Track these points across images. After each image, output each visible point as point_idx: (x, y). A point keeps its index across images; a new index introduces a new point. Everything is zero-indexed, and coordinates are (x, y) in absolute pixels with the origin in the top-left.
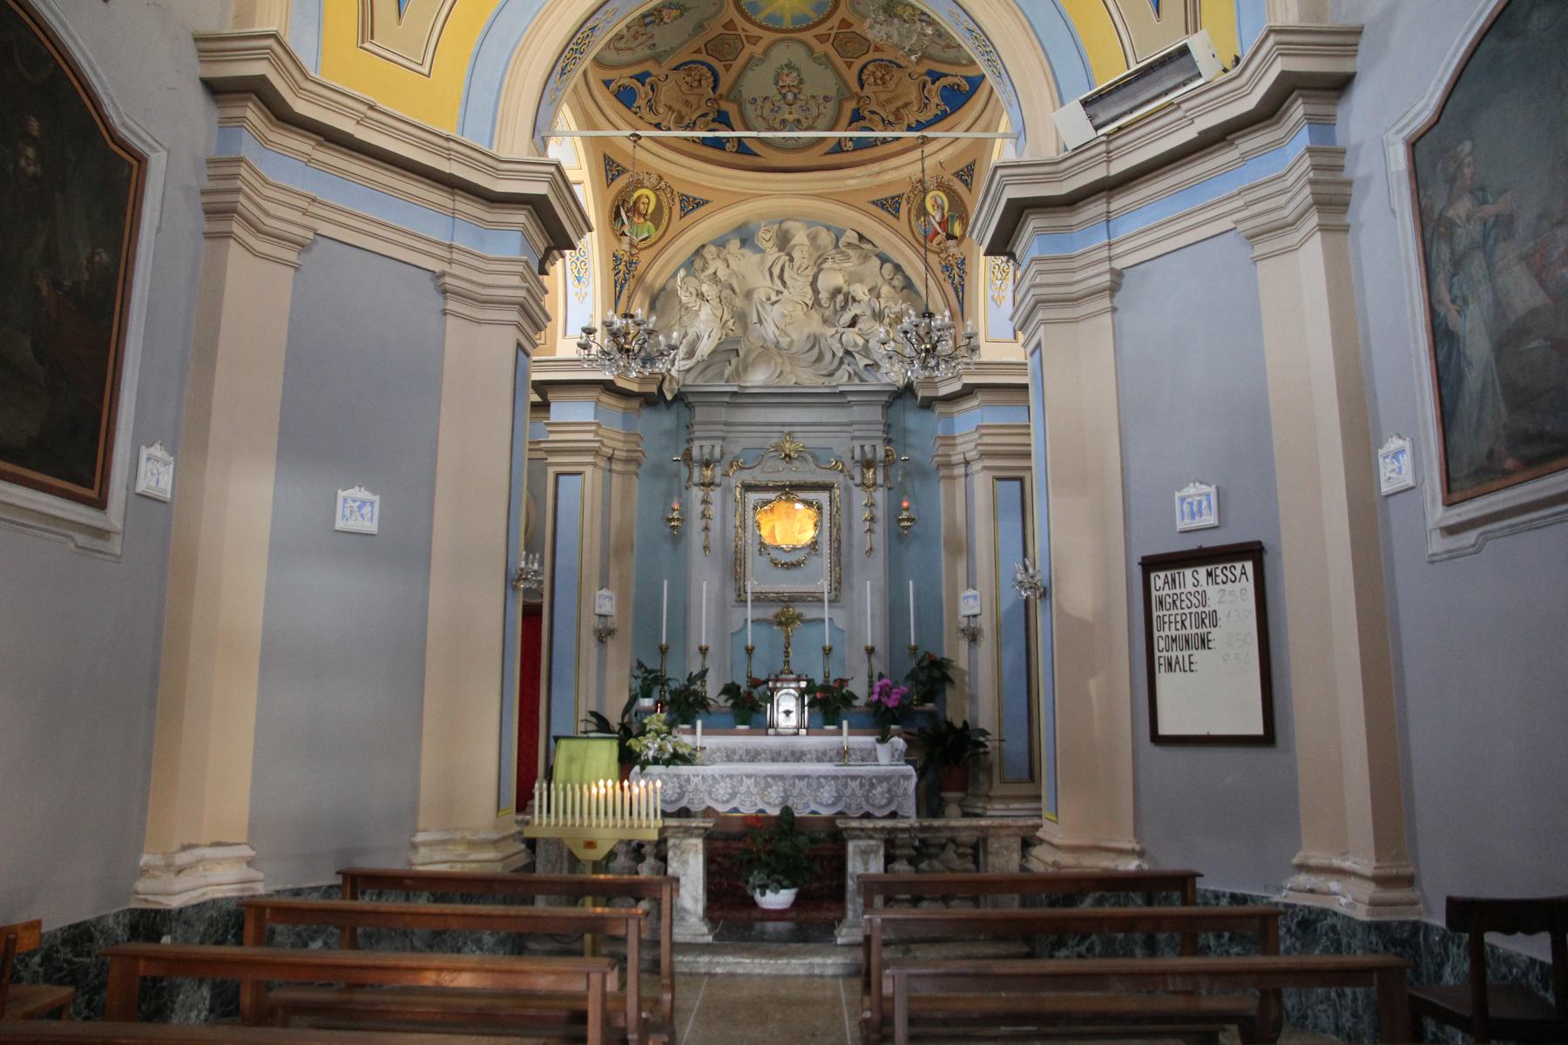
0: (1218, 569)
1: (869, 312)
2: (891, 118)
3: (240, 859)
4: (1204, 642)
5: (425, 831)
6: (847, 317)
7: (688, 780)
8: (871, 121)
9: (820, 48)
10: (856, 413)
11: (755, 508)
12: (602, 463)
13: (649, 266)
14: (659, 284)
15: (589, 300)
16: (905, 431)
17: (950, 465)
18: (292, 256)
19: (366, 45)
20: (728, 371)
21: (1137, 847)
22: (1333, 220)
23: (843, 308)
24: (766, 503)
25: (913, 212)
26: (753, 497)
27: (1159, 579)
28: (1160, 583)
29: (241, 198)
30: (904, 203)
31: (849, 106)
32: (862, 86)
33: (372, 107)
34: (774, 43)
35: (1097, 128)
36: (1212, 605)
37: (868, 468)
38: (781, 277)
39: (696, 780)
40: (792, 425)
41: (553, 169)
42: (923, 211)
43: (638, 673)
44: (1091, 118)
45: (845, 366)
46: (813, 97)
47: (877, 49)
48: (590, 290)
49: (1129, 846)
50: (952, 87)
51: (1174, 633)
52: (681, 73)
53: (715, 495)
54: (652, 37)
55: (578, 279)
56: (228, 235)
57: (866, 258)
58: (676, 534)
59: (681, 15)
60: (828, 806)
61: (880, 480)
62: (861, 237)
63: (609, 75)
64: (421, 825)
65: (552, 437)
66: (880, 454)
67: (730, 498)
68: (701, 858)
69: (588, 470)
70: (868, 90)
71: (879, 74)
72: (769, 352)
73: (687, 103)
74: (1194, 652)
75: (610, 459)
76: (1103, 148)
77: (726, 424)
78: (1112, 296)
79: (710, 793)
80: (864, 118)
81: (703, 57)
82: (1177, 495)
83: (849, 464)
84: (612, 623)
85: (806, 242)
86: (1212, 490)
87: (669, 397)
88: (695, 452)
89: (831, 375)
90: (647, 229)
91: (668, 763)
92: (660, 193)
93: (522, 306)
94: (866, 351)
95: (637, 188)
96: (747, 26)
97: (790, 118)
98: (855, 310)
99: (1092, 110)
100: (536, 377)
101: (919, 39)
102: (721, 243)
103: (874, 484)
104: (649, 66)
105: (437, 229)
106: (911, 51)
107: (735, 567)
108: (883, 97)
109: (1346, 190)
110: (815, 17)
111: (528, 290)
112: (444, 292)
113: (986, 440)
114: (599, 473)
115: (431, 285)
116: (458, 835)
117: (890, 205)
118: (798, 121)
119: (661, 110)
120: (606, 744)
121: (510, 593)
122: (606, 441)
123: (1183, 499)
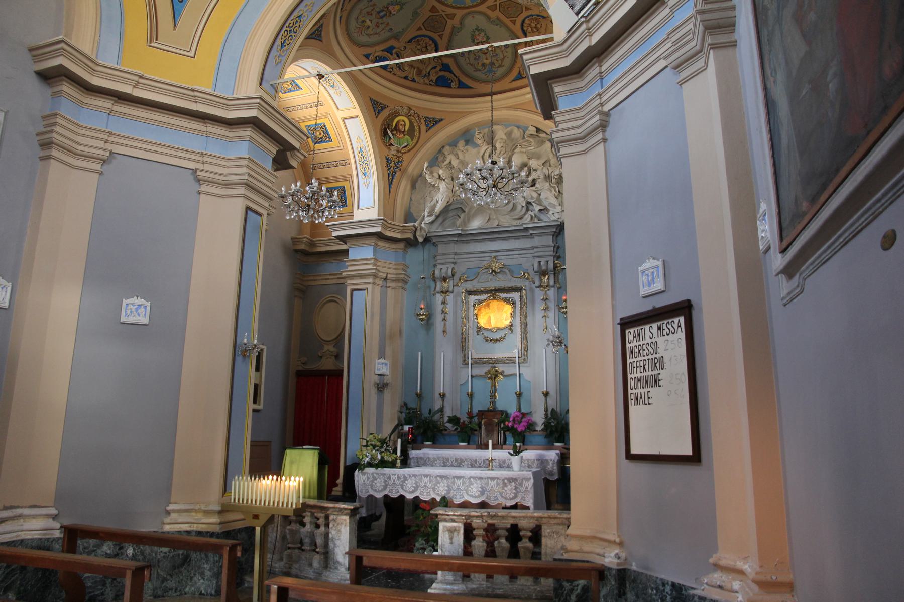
0: (664, 323)
1: (542, 177)
3: (48, 516)
4: (656, 381)
5: (175, 503)
7: (389, 478)
9: (493, 15)
10: (537, 241)
11: (474, 305)
13: (408, 165)
14: (416, 173)
15: (371, 187)
18: (98, 167)
19: (153, 44)
20: (458, 222)
21: (618, 540)
22: (722, 38)
24: (480, 302)
26: (473, 299)
27: (630, 333)
28: (631, 337)
29: (55, 135)
33: (141, 77)
34: (463, 18)
35: (577, 14)
36: (661, 352)
39: (394, 477)
43: (404, 410)
47: (527, 9)
48: (371, 180)
49: (611, 537)
51: (639, 375)
53: (450, 298)
54: (388, 24)
55: (364, 174)
56: (49, 157)
57: (543, 142)
58: (428, 321)
59: (401, 8)
60: (475, 497)
61: (552, 283)
62: (538, 130)
64: (172, 500)
65: (350, 268)
66: (551, 266)
67: (459, 300)
68: (348, 528)
69: (370, 287)
71: (533, 25)
74: (650, 389)
75: (386, 279)
76: (584, 26)
77: (456, 254)
79: (402, 486)
81: (424, 32)
82: (640, 269)
84: (387, 379)
85: (505, 137)
86: (659, 263)
87: (421, 240)
88: (437, 273)
89: (521, 218)
91: (377, 466)
93: (246, 184)
95: (396, 117)
96: (444, 8)
97: (487, 62)
98: (534, 175)
100: (334, 234)
102: (454, 144)
103: (548, 286)
104: (392, 42)
105: (196, 144)
107: (463, 343)
109: (731, 13)
112: (199, 180)
114: (378, 289)
115: (192, 177)
116: (197, 507)
119: (407, 68)
120: (311, 452)
121: (239, 359)
123: (643, 272)
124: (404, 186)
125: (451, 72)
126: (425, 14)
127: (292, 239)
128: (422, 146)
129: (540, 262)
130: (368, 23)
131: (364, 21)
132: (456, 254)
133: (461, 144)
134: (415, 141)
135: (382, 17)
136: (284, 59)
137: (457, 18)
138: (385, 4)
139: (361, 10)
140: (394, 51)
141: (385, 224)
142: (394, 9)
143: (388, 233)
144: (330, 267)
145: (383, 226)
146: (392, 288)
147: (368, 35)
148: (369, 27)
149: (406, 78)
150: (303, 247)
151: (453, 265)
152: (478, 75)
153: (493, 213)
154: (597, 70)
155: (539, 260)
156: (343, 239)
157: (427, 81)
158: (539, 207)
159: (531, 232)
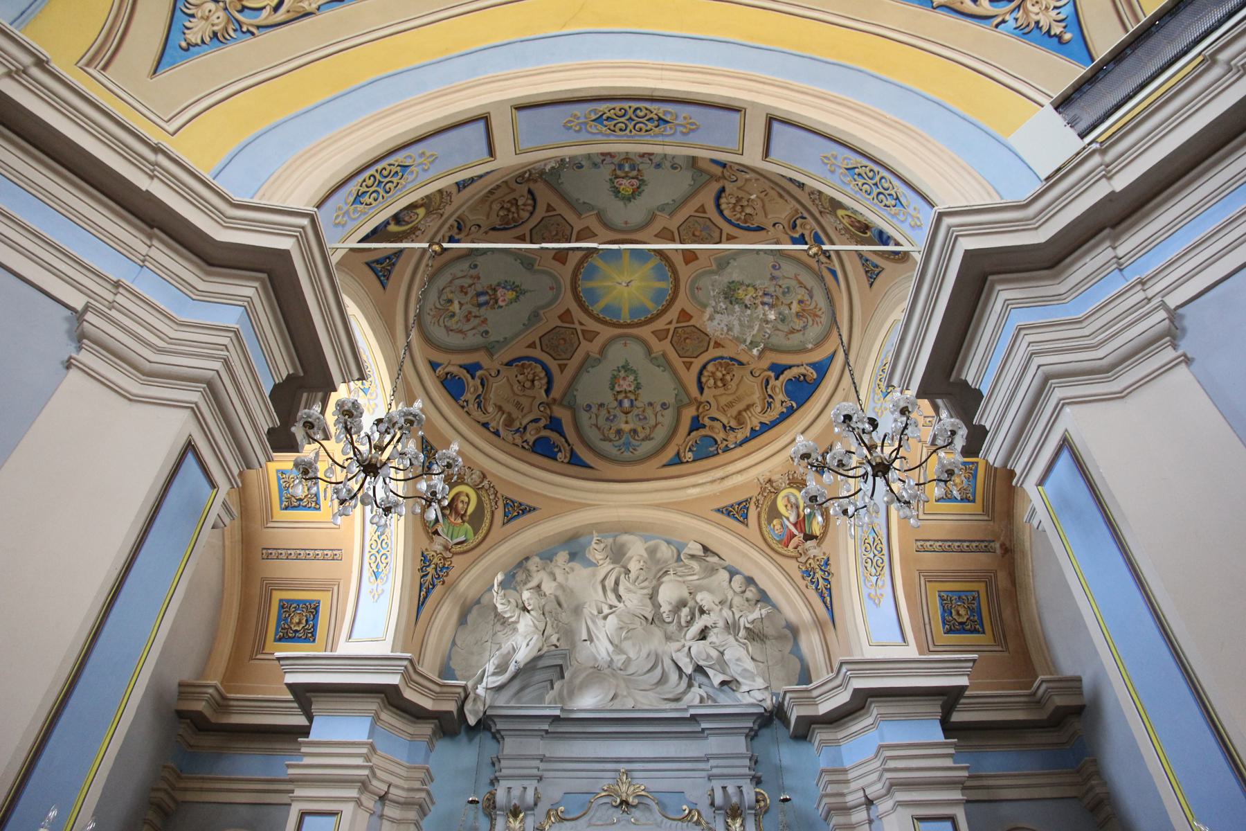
1: (721, 624)
2: (733, 424)
8: (712, 428)
9: (658, 347)
10: (713, 745)
12: (369, 802)
14: (472, 594)
15: (385, 600)
16: (779, 769)
17: (846, 810)
19: (90, 70)
23: (690, 623)
25: (764, 516)
31: (689, 413)
32: (701, 390)
37: (734, 818)
38: (615, 590)
40: (630, 761)
41: (305, 222)
42: (774, 513)
44: (1072, 123)
45: (695, 689)
46: (651, 404)
47: (718, 345)
48: (388, 587)
50: (797, 379)
52: (514, 370)
54: (485, 321)
55: (376, 575)
57: (713, 570)
59: (517, 299)
63: (438, 357)
65: (307, 761)
66: (750, 793)
69: (348, 809)
70: (708, 394)
71: (719, 375)
72: (597, 674)
73: (518, 405)
75: (383, 798)
76: (1097, 159)
77: (542, 759)
78: (868, 810)
80: (704, 426)
81: (537, 353)
83: (707, 812)
85: (645, 555)
87: (472, 721)
92: (483, 493)
93: (210, 385)
94: (722, 664)
97: (626, 428)
99: (1073, 111)
100: (291, 679)
101: (761, 329)
104: (480, 357)
106: (753, 344)
108: (724, 401)
110: (653, 308)
111: (226, 362)
113: (892, 764)
114: (363, 817)
117: (737, 512)
118: (635, 431)
119: (490, 409)
122: (378, 773)
124: (446, 614)
125: (562, 434)
126: (551, 320)
127: (181, 685)
128: (491, 549)
129: (724, 788)
131: (450, 301)
132: (542, 759)
133: (562, 556)
136: (351, 225)
137: (599, 341)
138: (494, 283)
139: (455, 278)
140: (479, 373)
141: (411, 669)
142: (505, 296)
143: (409, 694)
144: (251, 765)
145: (406, 676)
146: (393, 820)
147: (449, 330)
148: (453, 315)
149: (485, 425)
150: (200, 706)
151: (535, 782)
152: (607, 447)
153: (623, 685)
154: (1109, 253)
155: (724, 783)
156: (305, 696)
157: (518, 441)
158: (722, 678)
159: (704, 725)
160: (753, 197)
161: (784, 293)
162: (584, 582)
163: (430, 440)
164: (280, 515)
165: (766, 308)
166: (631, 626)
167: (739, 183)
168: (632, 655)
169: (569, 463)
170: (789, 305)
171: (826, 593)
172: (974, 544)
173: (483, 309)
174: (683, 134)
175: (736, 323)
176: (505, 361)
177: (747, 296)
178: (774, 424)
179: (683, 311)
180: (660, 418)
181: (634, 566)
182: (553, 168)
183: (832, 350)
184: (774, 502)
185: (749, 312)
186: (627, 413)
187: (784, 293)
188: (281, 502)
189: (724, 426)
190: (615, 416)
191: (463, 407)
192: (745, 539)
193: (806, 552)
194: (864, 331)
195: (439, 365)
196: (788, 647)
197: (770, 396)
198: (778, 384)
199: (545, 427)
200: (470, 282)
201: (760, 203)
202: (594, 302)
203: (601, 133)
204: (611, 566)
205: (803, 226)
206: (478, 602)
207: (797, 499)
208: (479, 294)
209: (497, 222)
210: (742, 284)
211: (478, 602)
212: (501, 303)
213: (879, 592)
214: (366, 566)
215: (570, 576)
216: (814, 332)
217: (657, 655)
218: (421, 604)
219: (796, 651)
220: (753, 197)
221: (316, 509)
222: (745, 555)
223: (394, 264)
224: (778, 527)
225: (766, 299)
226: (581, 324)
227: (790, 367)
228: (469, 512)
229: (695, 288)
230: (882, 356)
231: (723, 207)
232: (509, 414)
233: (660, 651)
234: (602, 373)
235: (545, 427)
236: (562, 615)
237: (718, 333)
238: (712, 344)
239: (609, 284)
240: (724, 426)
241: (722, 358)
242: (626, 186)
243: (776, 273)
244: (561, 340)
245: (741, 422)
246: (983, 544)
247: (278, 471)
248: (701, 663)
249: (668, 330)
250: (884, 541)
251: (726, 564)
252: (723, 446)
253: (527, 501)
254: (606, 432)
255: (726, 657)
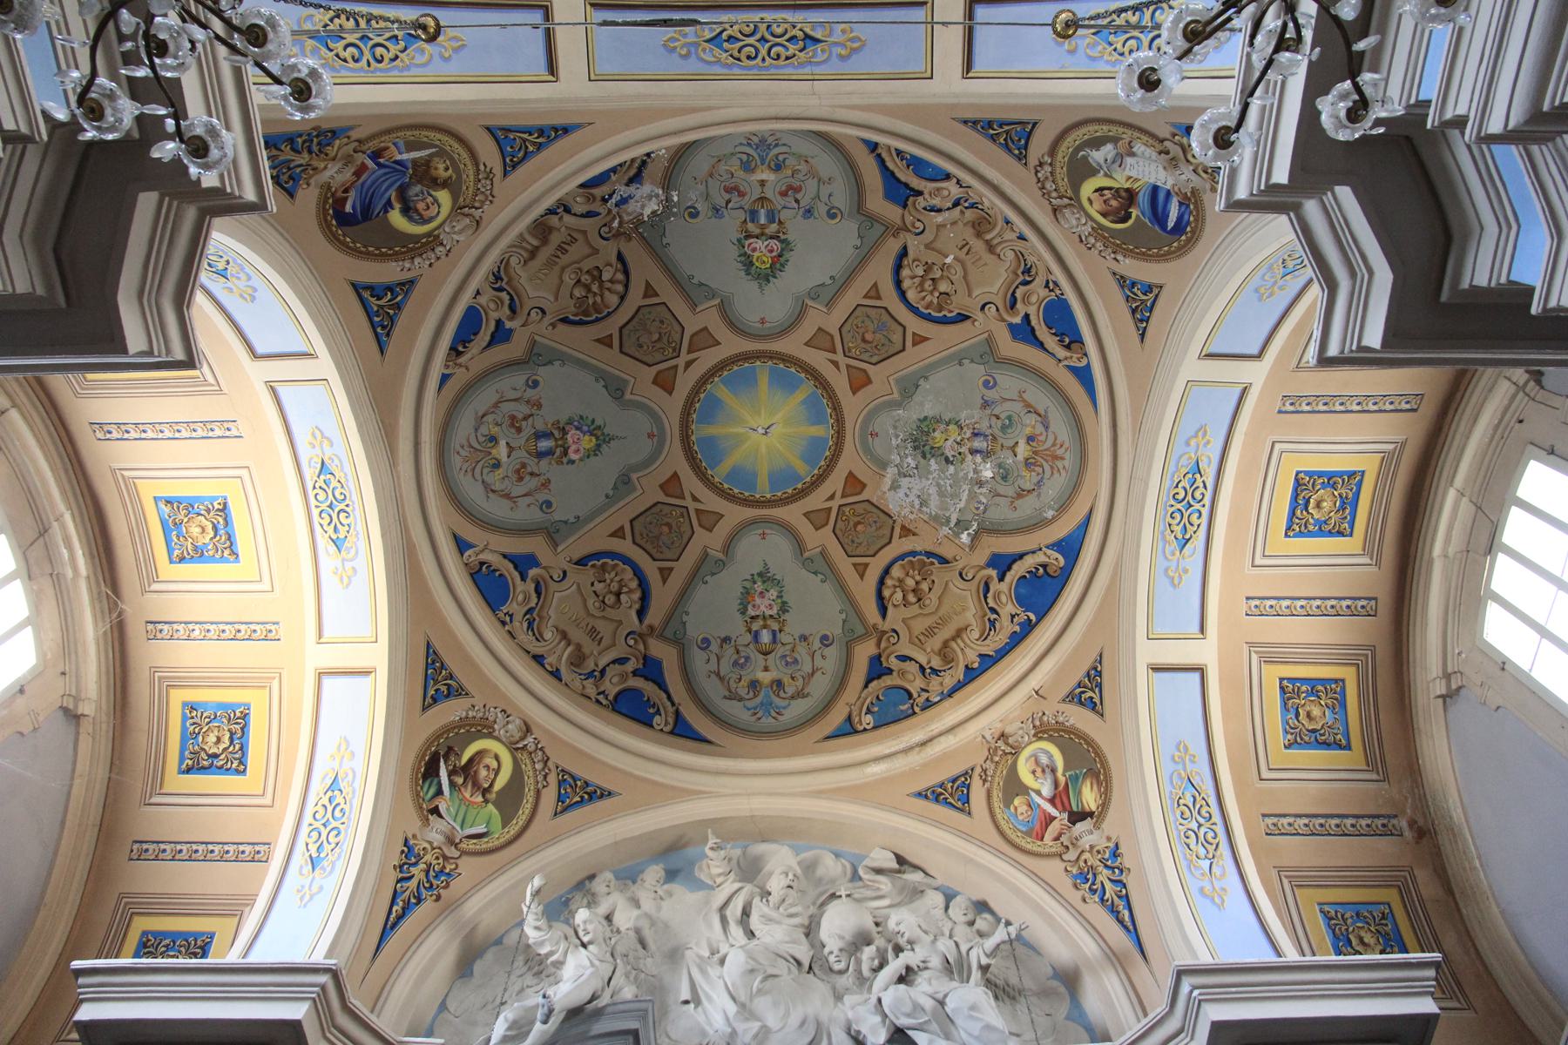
1: (935, 962)
2: (936, 663)
6: (895, 966)
25: (997, 795)
30: (976, 783)
31: (864, 652)
32: (883, 611)
42: (1014, 787)
46: (804, 638)
47: (907, 532)
48: (330, 883)
52: (588, 574)
54: (546, 484)
57: (917, 893)
62: (901, 860)
71: (910, 583)
73: (593, 633)
80: (890, 671)
81: (625, 547)
85: (799, 871)
90: (486, 817)
95: (479, 735)
97: (765, 678)
100: (86, 1013)
101: (972, 496)
106: (961, 525)
108: (919, 626)
110: (805, 472)
117: (951, 794)
118: (779, 683)
119: (548, 635)
124: (430, 950)
125: (662, 686)
126: (648, 492)
130: (501, 451)
131: (493, 439)
134: (513, 829)
135: (540, 455)
137: (723, 529)
138: (564, 419)
140: (533, 572)
145: (320, 1003)
148: (497, 465)
149: (538, 659)
152: (736, 710)
160: (949, 260)
161: (1004, 428)
162: (688, 914)
163: (442, 652)
164: (176, 781)
165: (978, 458)
166: (771, 971)
167: (928, 236)
168: (772, 1021)
169: (672, 733)
170: (1013, 449)
171: (1121, 905)
172: (1364, 822)
173: (544, 462)
174: (842, 58)
175: (933, 490)
176: (576, 557)
177: (947, 440)
178: (1002, 653)
179: (851, 476)
180: (819, 662)
181: (776, 885)
182: (654, 212)
183: (1086, 510)
184: (1013, 769)
185: (952, 469)
186: (766, 654)
187: (1004, 428)
188: (182, 759)
189: (922, 669)
190: (747, 658)
191: (504, 623)
192: (967, 836)
193: (1075, 842)
194: (1138, 427)
195: (471, 546)
196: (1063, 1009)
197: (993, 610)
198: (1003, 589)
199: (635, 673)
200: (525, 410)
201: (959, 269)
202: (716, 462)
203: (719, 61)
204: (737, 885)
205: (1026, 297)
206: (499, 942)
207: (1051, 757)
208: (539, 436)
209: (570, 310)
210: (938, 420)
211: (499, 942)
212: (573, 456)
213: (1217, 884)
214: (300, 846)
215: (664, 904)
216: (1055, 486)
217: (819, 1025)
218: (389, 927)
219: (1077, 1013)
220: (949, 260)
221: (238, 772)
222: (969, 861)
223: (398, 307)
224: (1023, 809)
225: (978, 444)
226: (695, 499)
227: (1021, 556)
228: (498, 786)
229: (869, 434)
230: (1172, 468)
231: (906, 284)
232: (579, 647)
233: (824, 1018)
234: (728, 584)
235: (635, 673)
236: (650, 951)
237: (906, 512)
238: (897, 530)
239: (740, 430)
240: (922, 669)
241: (913, 553)
242: (762, 251)
243: (991, 395)
244: (662, 527)
245: (945, 653)
246: (1379, 822)
247: (185, 704)
248: (903, 1021)
249: (830, 509)
250: (1212, 800)
251: (938, 882)
252: (921, 700)
253: (597, 779)
254: (733, 685)
255: (950, 1005)
